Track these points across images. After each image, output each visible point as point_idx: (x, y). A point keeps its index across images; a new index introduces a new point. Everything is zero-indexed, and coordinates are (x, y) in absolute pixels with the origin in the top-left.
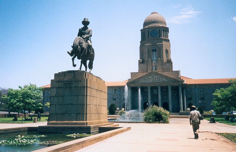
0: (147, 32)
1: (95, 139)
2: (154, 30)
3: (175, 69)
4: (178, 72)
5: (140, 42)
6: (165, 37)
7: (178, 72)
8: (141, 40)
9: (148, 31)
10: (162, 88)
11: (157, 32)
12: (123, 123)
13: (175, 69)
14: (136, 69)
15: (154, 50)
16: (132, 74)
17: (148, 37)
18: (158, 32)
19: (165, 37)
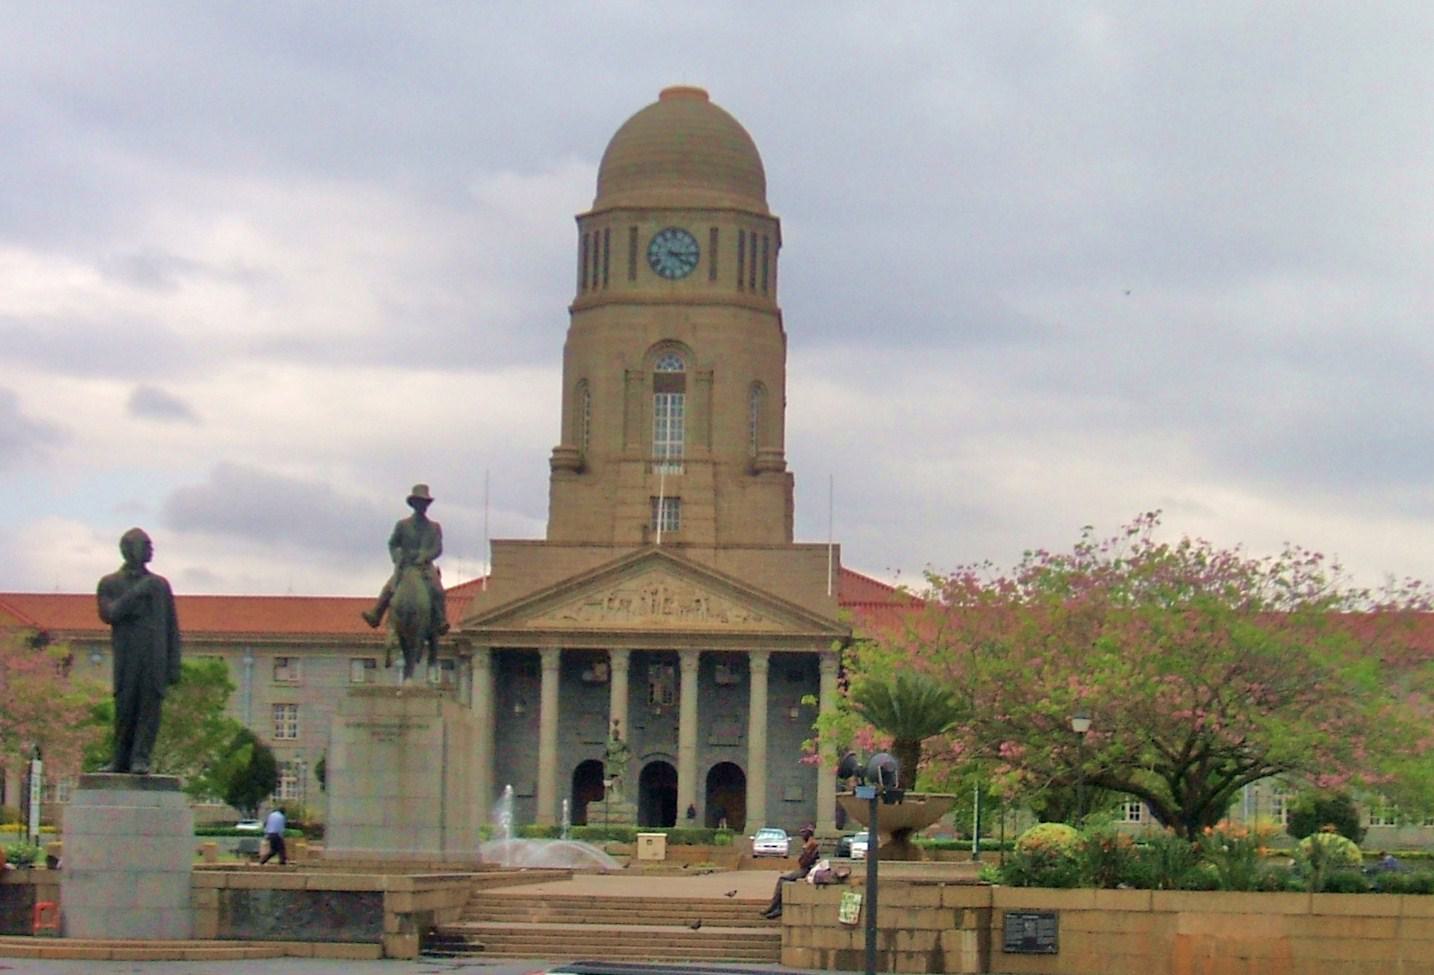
2: (674, 231)
11: (694, 241)
15: (669, 384)
17: (633, 275)
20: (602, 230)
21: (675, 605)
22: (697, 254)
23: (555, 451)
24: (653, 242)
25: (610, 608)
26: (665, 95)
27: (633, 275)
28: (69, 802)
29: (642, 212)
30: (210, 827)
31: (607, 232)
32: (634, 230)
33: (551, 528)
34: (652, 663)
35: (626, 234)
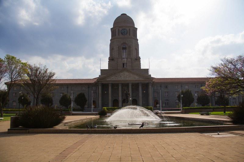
0: (117, 31)
1: (138, 127)
2: (124, 29)
3: (143, 67)
4: (147, 71)
5: (110, 40)
6: (134, 30)
7: (147, 71)
8: (110, 42)
9: (119, 29)
10: (133, 85)
11: (127, 30)
12: (130, 135)
13: (143, 67)
14: (106, 66)
15: (124, 49)
16: (102, 71)
17: (119, 35)
18: (128, 31)
19: (134, 30)
20: (114, 29)
21: (128, 76)
22: (127, 32)
23: (9, 129)
24: (121, 31)
25: (119, 77)
26: (122, 15)
27: (119, 35)
28: (120, 33)
29: (120, 27)
30: (116, 108)
31: (115, 30)
32: (119, 29)
33: (11, 128)
34: (125, 85)
35: (118, 30)
